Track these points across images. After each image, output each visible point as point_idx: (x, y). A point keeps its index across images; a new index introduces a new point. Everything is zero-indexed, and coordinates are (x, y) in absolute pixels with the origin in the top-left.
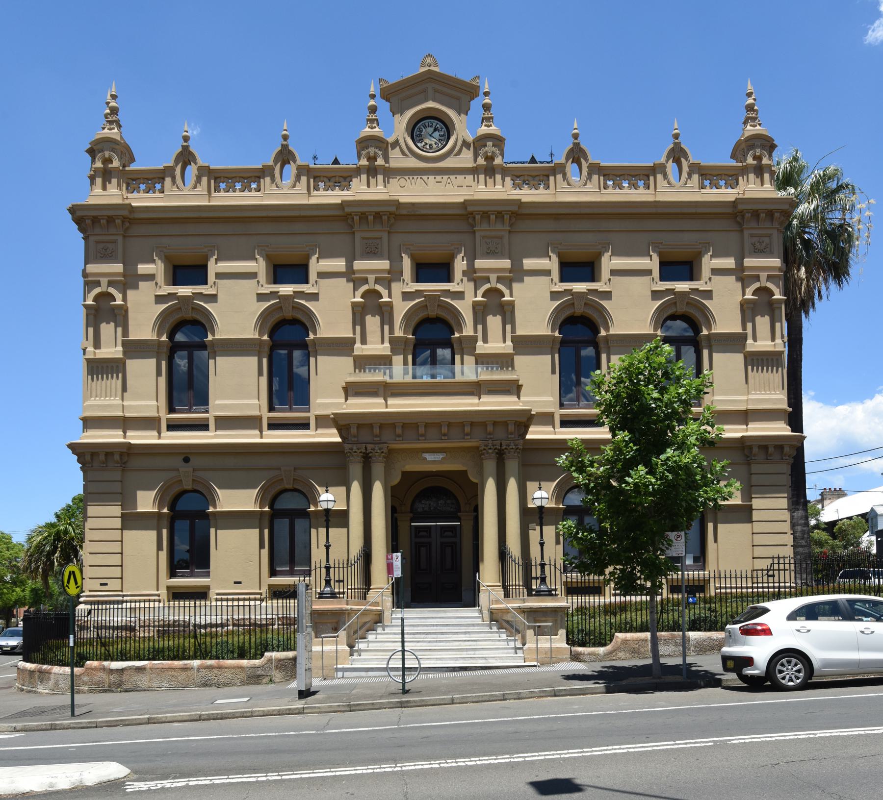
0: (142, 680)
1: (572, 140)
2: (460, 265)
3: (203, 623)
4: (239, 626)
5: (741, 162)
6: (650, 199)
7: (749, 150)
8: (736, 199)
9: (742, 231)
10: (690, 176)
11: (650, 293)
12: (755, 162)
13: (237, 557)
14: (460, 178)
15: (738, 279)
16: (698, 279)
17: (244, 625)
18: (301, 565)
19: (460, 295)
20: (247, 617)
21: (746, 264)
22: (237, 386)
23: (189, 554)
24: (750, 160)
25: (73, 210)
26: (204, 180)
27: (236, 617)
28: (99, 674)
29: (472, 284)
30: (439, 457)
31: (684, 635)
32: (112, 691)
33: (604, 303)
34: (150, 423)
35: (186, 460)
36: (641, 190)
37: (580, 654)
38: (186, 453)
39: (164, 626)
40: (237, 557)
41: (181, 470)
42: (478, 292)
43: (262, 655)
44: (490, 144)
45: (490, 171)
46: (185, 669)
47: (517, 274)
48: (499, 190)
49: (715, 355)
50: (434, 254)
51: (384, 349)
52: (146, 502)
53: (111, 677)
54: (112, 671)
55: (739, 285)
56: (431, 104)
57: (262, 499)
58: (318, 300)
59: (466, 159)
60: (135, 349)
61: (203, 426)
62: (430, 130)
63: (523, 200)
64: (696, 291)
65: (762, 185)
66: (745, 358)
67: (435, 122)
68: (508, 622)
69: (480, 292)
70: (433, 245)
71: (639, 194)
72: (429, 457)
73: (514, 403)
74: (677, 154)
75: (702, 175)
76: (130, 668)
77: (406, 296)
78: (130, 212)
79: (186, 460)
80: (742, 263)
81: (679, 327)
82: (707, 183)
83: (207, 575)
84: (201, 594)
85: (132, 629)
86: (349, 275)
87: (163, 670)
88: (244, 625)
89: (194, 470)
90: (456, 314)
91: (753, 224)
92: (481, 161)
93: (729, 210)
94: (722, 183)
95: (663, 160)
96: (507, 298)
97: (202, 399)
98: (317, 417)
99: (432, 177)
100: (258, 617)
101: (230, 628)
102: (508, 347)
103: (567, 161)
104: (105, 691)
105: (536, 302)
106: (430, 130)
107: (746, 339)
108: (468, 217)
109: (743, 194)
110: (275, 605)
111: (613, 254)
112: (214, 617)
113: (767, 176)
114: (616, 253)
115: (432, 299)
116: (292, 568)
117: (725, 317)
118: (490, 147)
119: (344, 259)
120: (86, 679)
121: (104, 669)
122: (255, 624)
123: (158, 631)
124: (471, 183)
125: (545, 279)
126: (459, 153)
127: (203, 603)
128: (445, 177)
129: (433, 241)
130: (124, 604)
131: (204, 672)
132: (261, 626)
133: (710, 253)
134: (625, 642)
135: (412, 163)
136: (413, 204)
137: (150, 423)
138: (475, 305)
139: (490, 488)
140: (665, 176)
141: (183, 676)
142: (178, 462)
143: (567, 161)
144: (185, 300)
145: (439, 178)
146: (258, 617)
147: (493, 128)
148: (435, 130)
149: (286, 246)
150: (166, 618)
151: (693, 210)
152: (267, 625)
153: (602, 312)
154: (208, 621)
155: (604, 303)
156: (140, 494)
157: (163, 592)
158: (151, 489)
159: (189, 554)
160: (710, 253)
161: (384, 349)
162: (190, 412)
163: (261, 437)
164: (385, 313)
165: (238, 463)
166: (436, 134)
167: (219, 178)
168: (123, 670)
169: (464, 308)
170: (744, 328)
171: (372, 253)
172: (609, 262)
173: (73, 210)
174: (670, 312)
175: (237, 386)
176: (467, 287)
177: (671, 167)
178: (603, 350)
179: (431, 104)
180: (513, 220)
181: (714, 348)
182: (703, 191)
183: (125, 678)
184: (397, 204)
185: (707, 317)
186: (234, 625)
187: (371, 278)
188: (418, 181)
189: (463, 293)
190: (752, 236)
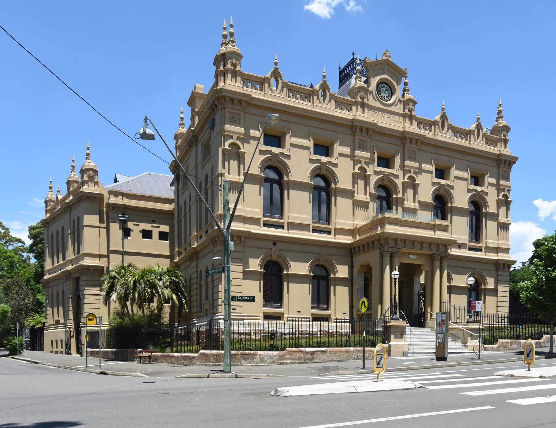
0: (325, 357)
1: (274, 65)
2: (398, 161)
3: (286, 332)
4: (301, 334)
5: (354, 99)
6: (468, 145)
7: (502, 132)
8: (353, 119)
9: (499, 168)
10: (330, 101)
11: (467, 189)
12: (232, 68)
13: (298, 296)
14: (398, 117)
15: (497, 189)
16: (283, 148)
17: (304, 334)
18: (323, 304)
19: (397, 177)
20: (265, 329)
21: (356, 154)
22: (299, 207)
23: (273, 294)
24: (358, 99)
25: (517, 159)
26: (285, 89)
27: (300, 329)
28: (298, 354)
29: (402, 172)
30: (415, 257)
31: (552, 337)
32: (307, 363)
33: (334, 169)
34: (255, 221)
35: (275, 244)
36: (428, 132)
37: (486, 348)
38: (275, 241)
39: (266, 333)
40: (298, 296)
41: (273, 249)
42: (226, 143)
43: (284, 349)
44: (411, 104)
45: (411, 117)
46: (347, 351)
47: (420, 171)
48: (413, 128)
49: (453, 217)
50: (387, 154)
51: (367, 198)
52: (255, 265)
53: (306, 356)
54: (307, 353)
55: (496, 191)
56: (385, 76)
57: (311, 269)
58: (337, 167)
59: (399, 108)
60: (249, 178)
61: (280, 226)
62: (384, 89)
63: (253, 96)
64: (282, 154)
65: (236, 82)
66: (498, 224)
67: (388, 88)
68: (452, 334)
69: (406, 177)
70: (387, 149)
71: (305, 105)
72: (412, 257)
73: (432, 235)
74: (276, 74)
75: (289, 90)
76: (318, 351)
77: (376, 173)
78: (251, 99)
79: (275, 244)
80: (354, 153)
81: (273, 175)
82: (291, 94)
83: (281, 307)
84: (278, 317)
85: (249, 334)
86: (352, 157)
87: (336, 352)
88: (304, 334)
89: (279, 250)
90: (395, 185)
91: (230, 106)
92: (407, 111)
93: (496, 158)
94: (298, 96)
95: (268, 75)
96: (242, 150)
97: (281, 212)
98: (289, 224)
99: (386, 114)
100: (311, 330)
101: (297, 335)
102: (241, 178)
103: (271, 77)
104: (303, 363)
105: (427, 186)
106: (384, 89)
107: (498, 216)
108: (403, 138)
109: (355, 116)
110: (319, 324)
111: (339, 145)
112: (288, 329)
113: (238, 78)
114: (456, 169)
115: (386, 176)
116: (318, 305)
117: (344, 181)
118: (410, 106)
119: (349, 148)
120: (288, 357)
121: (302, 351)
122: (309, 334)
123: (263, 336)
124: (402, 121)
125: (307, 152)
126: (396, 105)
127: (281, 322)
128: (392, 116)
129: (390, 147)
130: (245, 321)
131: (357, 353)
132: (312, 334)
133: (290, 134)
134: (503, 343)
135: (377, 104)
136: (382, 127)
137: (255, 221)
138: (404, 183)
139: (438, 272)
140: (269, 85)
141: (346, 355)
142: (270, 245)
143: (271, 77)
144: (275, 155)
145: (389, 115)
146: (311, 330)
147: (235, 47)
148: (386, 90)
149: (325, 136)
150: (267, 329)
151: (484, 155)
152: (315, 334)
153: (450, 195)
154: (288, 331)
155: (286, 161)
156: (251, 260)
157: (262, 315)
158: (257, 258)
159: (273, 294)
160: (290, 134)
161: (367, 198)
162: (271, 217)
163: (335, 239)
164: (366, 178)
165: (301, 248)
166: (387, 92)
167: (457, 132)
168: (314, 352)
169: (399, 182)
170: (354, 187)
171: (363, 148)
172: (290, 139)
173: (517, 159)
174: (269, 164)
175: (299, 207)
176: (400, 173)
177: (273, 81)
178: (285, 188)
179: (385, 76)
180: (246, 106)
181: (453, 213)
182: (289, 99)
183: (315, 356)
184: (375, 125)
185: (486, 204)
186: (299, 334)
187: (235, 136)
188: (380, 114)
189: (289, 156)
190: (502, 171)
